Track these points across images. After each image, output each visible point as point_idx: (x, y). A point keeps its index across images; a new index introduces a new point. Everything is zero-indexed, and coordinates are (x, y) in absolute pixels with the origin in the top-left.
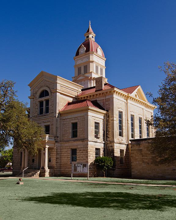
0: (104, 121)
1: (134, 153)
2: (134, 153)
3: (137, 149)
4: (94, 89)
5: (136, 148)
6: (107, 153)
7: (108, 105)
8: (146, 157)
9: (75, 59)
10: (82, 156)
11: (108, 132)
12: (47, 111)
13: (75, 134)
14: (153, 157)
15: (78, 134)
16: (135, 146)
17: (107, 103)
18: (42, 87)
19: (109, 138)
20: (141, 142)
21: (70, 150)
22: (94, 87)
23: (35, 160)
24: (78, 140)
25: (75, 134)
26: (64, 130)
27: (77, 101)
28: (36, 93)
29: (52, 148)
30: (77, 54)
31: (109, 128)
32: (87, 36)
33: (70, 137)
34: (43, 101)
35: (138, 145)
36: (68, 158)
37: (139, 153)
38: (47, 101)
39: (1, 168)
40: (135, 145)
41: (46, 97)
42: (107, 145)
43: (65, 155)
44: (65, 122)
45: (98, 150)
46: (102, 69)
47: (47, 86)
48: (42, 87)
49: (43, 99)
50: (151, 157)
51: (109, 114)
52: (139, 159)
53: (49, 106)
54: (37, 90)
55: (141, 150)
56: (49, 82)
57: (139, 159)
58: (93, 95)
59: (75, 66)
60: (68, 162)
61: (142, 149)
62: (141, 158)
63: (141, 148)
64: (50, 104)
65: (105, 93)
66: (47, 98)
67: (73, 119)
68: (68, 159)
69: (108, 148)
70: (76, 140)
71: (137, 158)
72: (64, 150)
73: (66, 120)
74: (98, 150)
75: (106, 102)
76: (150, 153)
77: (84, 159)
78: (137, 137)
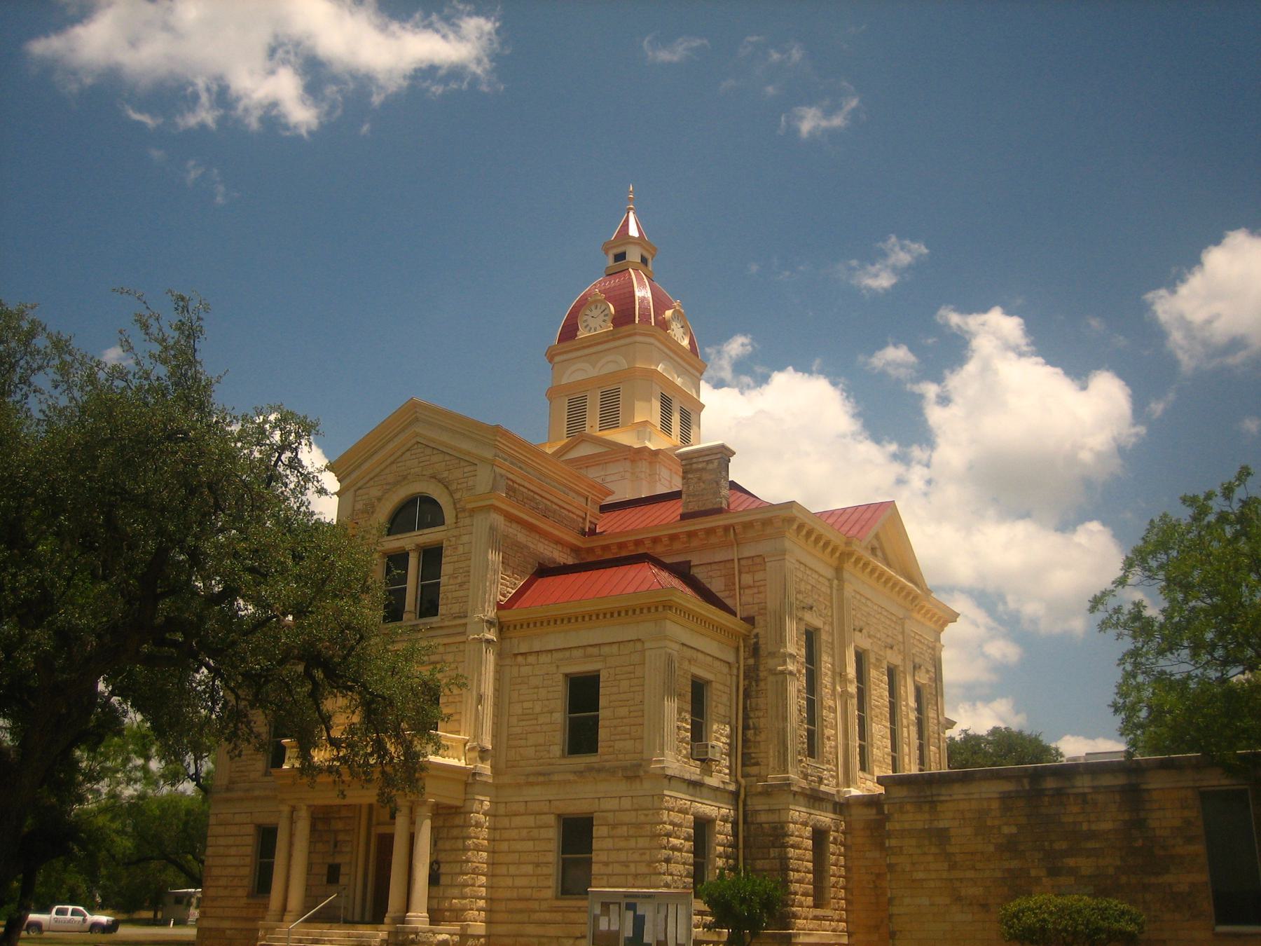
0: (735, 671)
1: (901, 847)
2: (901, 847)
3: (919, 825)
4: (676, 509)
5: (912, 819)
6: (744, 848)
7: (755, 590)
8: (970, 874)
9: (557, 359)
10: (623, 856)
11: (755, 734)
12: (429, 606)
13: (582, 738)
14: (1009, 870)
15: (603, 734)
16: (907, 812)
17: (747, 579)
18: (405, 478)
19: (757, 764)
20: (943, 791)
21: (551, 820)
22: (675, 495)
23: (343, 870)
24: (599, 771)
25: (582, 738)
26: (517, 709)
27: (577, 562)
28: (370, 510)
29: (451, 807)
30: (569, 332)
31: (757, 713)
32: (619, 250)
33: (557, 750)
34: (407, 554)
35: (926, 808)
36: (537, 865)
37: (934, 850)
38: (432, 556)
39: (1256, 755)
40: (908, 807)
41: (426, 531)
42: (745, 805)
43: (519, 846)
44: (525, 670)
45: (702, 826)
46: (669, 401)
47: (433, 477)
48: (405, 478)
49: (408, 541)
50: (999, 874)
51: (757, 636)
52: (932, 884)
53: (443, 580)
54: (375, 492)
55: (941, 836)
56: (447, 458)
57: (932, 884)
58: (673, 538)
59: (553, 393)
60: (540, 888)
61: (947, 829)
62: (945, 875)
63: (942, 824)
64: (446, 569)
65: (739, 529)
66: (429, 536)
67: (576, 653)
68: (539, 871)
69: (749, 819)
70: (590, 769)
71: (920, 875)
72: (518, 818)
73: (531, 659)
74: (702, 826)
75: (740, 572)
76: (991, 848)
77: (636, 876)
78: (911, 768)
